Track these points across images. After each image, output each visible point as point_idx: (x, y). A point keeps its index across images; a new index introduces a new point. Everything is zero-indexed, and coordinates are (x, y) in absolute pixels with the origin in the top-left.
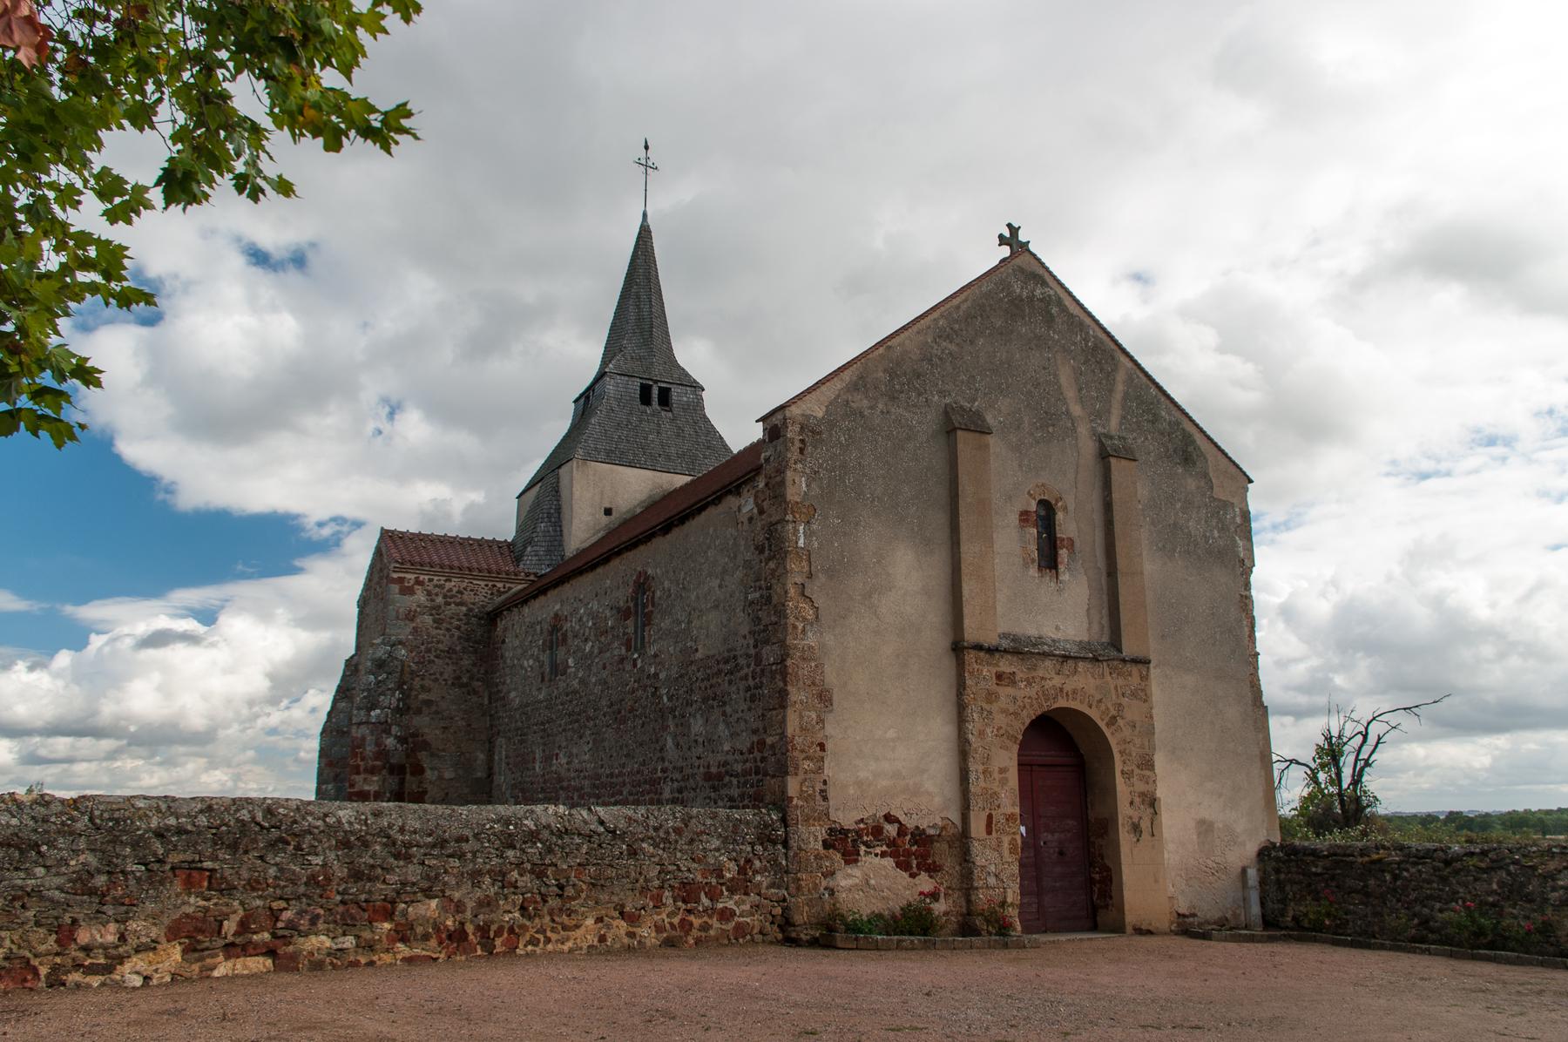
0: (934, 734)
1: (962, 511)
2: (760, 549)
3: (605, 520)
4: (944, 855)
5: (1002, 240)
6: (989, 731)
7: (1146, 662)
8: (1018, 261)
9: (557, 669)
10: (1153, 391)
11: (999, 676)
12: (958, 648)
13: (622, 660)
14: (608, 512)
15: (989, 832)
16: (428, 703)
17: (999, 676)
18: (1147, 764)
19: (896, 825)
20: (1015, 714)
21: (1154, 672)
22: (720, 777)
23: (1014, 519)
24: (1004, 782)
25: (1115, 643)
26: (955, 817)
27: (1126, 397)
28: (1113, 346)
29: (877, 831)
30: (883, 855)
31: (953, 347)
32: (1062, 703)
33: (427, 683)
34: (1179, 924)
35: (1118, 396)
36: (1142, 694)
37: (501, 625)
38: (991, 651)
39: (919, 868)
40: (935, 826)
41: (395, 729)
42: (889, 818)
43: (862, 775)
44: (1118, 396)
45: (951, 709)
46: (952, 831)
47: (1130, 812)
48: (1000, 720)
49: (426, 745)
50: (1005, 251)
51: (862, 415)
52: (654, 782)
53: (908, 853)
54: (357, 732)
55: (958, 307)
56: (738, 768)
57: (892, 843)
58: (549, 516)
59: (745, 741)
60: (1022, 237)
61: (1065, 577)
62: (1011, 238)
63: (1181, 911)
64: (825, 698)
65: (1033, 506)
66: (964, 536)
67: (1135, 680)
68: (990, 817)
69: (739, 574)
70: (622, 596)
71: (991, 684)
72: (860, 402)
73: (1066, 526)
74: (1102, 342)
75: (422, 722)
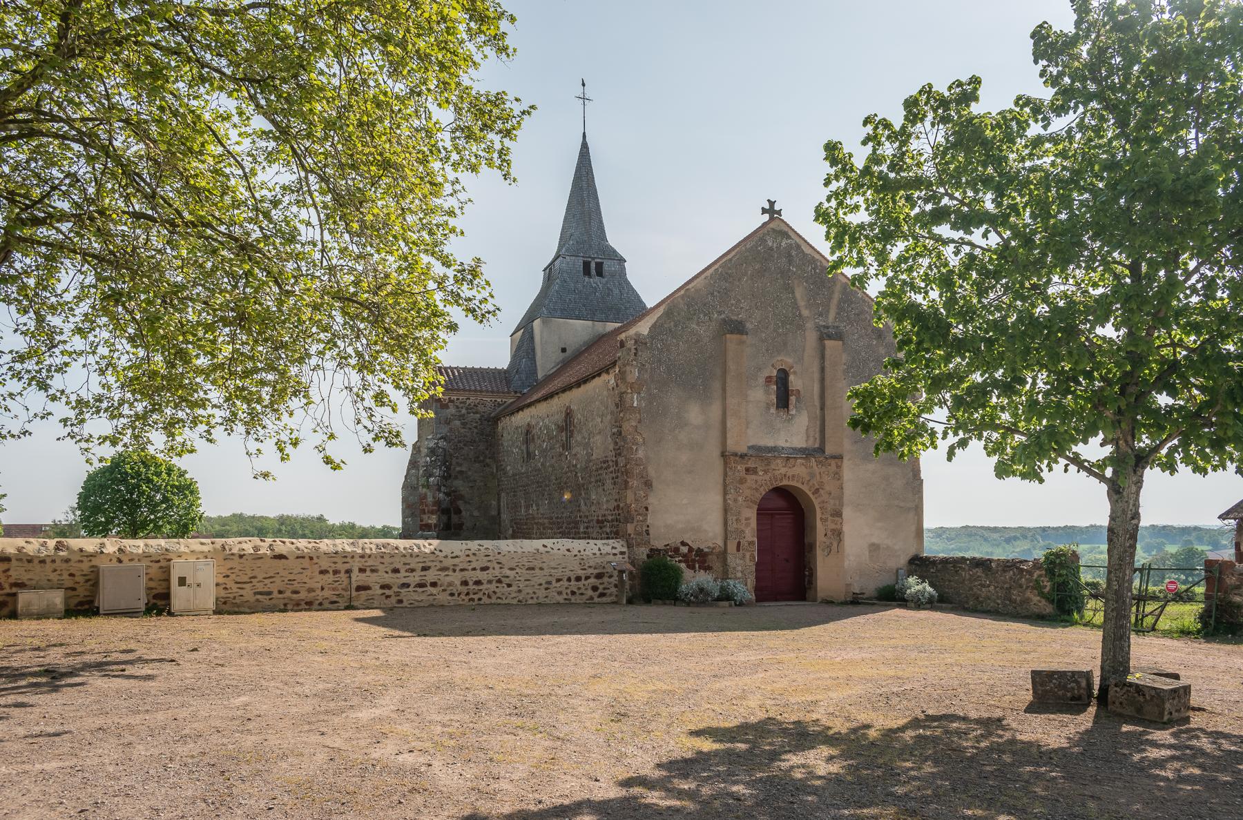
0: (712, 501)
1: (728, 380)
2: (617, 405)
3: (562, 356)
4: (713, 561)
5: (764, 211)
7: (840, 457)
8: (771, 225)
9: (530, 455)
11: (747, 470)
12: (723, 455)
13: (561, 455)
14: (564, 350)
15: (738, 550)
16: (461, 472)
17: (747, 470)
18: (838, 514)
20: (756, 489)
21: (845, 460)
22: (602, 522)
23: (761, 380)
24: (748, 525)
25: (821, 450)
26: (720, 542)
27: (839, 302)
29: (676, 550)
32: (785, 482)
33: (460, 461)
35: (835, 301)
36: (837, 476)
37: (500, 425)
38: (743, 456)
41: (443, 488)
42: (683, 544)
44: (835, 301)
45: (720, 487)
46: (717, 550)
47: (825, 539)
48: (748, 492)
49: (461, 497)
50: (766, 217)
52: (576, 523)
53: (694, 561)
54: (423, 491)
55: (730, 260)
56: (610, 518)
57: (684, 556)
58: (528, 354)
59: (613, 504)
60: (777, 208)
61: (793, 412)
62: (771, 210)
64: (648, 484)
65: (775, 373)
66: (728, 394)
67: (833, 468)
68: (739, 543)
69: (609, 417)
70: (560, 418)
71: (743, 473)
73: (795, 382)
75: (458, 484)
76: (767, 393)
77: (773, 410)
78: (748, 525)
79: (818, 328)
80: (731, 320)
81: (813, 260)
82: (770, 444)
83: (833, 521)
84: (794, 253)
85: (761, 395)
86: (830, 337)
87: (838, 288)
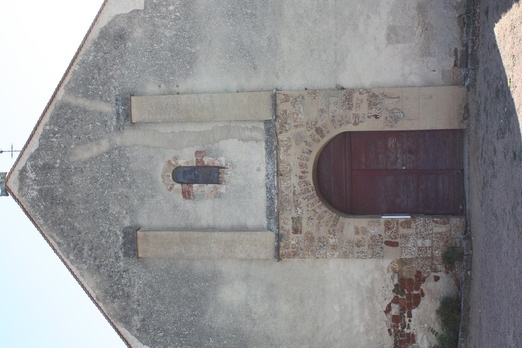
6: (332, 241)
8: (16, 193)
10: (75, 67)
11: (296, 231)
17: (296, 231)
19: (392, 305)
20: (320, 218)
23: (188, 204)
24: (365, 231)
27: (86, 95)
28: (52, 107)
29: (396, 319)
30: (410, 316)
31: (86, 248)
32: (309, 178)
34: (461, 66)
38: (279, 237)
39: (417, 288)
40: (392, 278)
42: (388, 309)
43: (362, 329)
47: (382, 119)
48: (323, 231)
51: (143, 320)
53: (409, 296)
55: (59, 244)
57: (402, 310)
61: (222, 161)
63: (452, 64)
65: (178, 186)
71: (301, 237)
72: (136, 319)
73: (187, 158)
74: (52, 118)
76: (202, 197)
77: (222, 189)
78: (365, 231)
79: (119, 129)
80: (124, 244)
81: (45, 136)
82: (262, 193)
83: (358, 106)
84: (41, 163)
85: (206, 206)
86: (128, 115)
87: (72, 100)
